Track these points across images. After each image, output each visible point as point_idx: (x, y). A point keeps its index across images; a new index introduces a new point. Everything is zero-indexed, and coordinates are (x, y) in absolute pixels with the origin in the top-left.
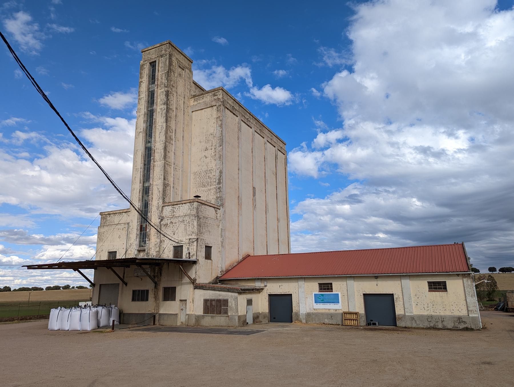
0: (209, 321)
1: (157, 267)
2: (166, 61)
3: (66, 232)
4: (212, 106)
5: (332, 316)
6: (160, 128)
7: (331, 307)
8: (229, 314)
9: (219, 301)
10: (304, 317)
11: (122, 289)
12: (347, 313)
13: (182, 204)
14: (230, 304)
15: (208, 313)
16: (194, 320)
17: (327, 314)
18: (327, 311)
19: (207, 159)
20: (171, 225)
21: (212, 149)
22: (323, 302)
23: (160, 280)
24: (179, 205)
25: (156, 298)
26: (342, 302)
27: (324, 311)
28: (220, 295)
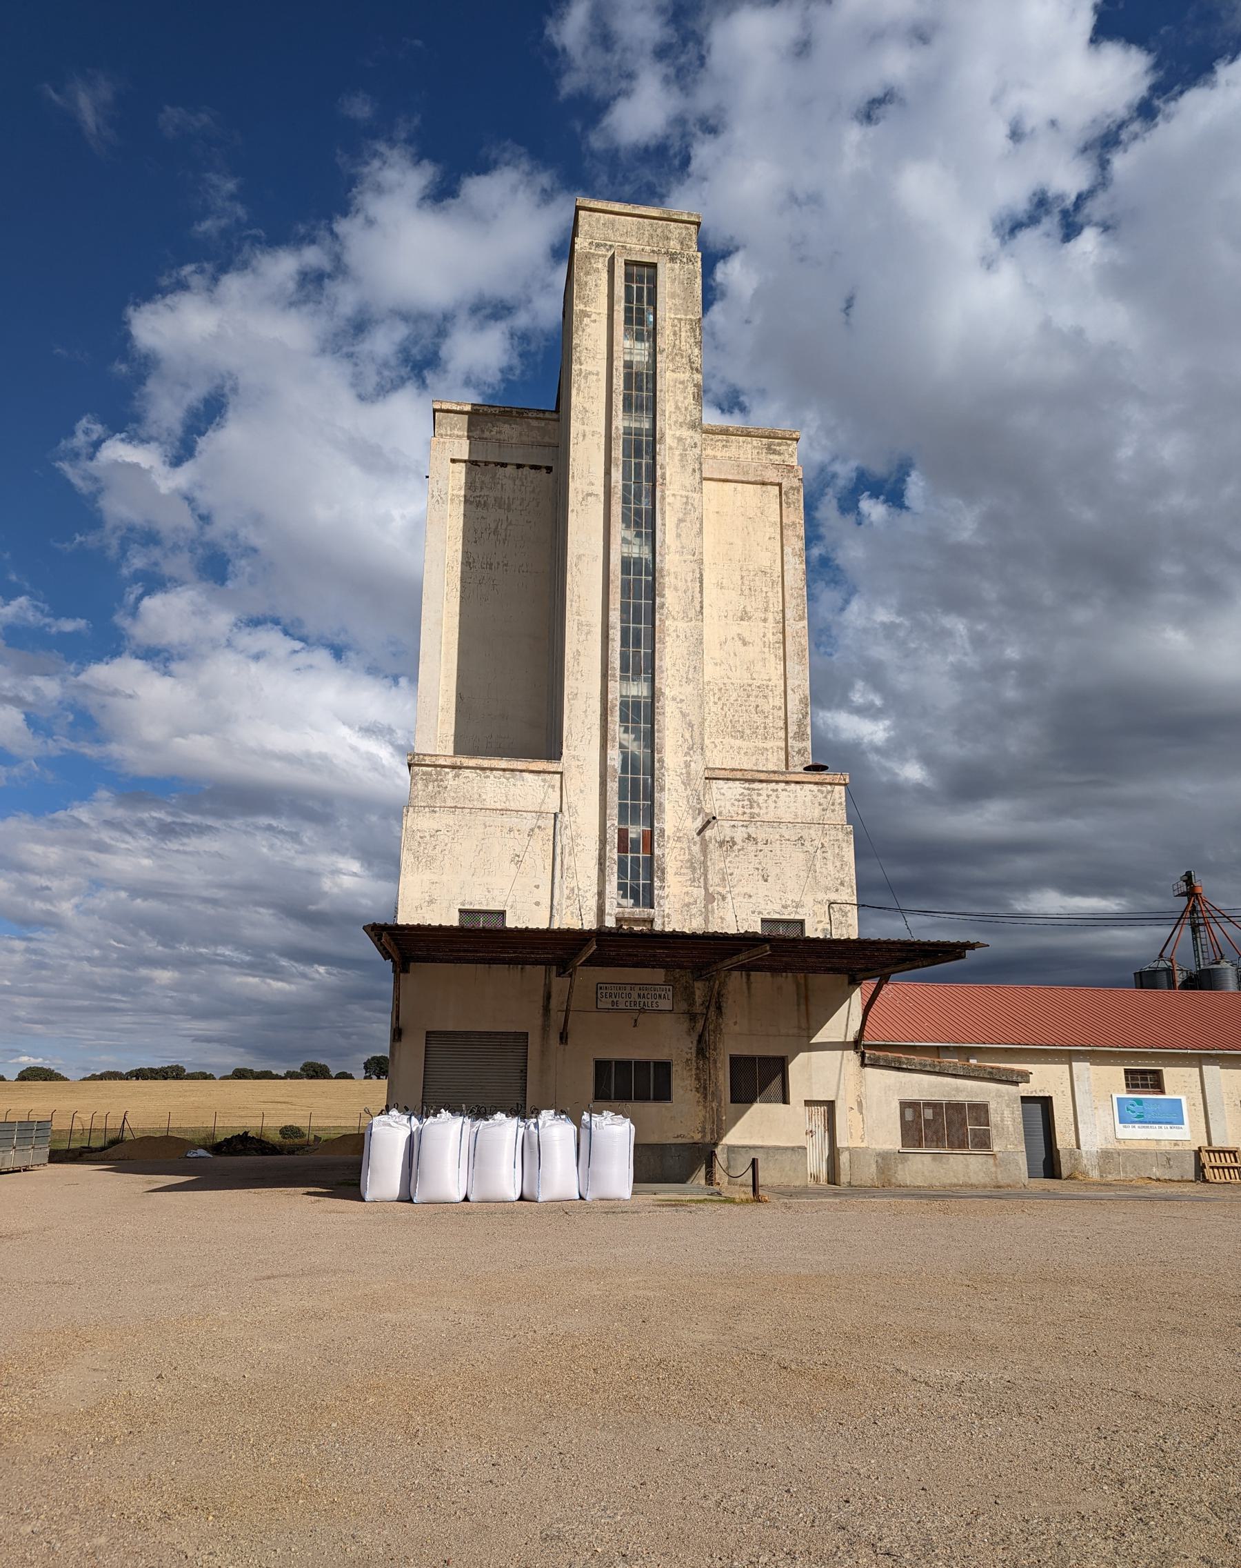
0: (923, 1167)
1: (698, 985)
2: (690, 281)
3: (203, 813)
4: (764, 484)
5: (1169, 1160)
6: (678, 503)
7: (1163, 1135)
8: (996, 1149)
9: (956, 1107)
10: (1095, 1161)
11: (543, 1053)
12: (1224, 1152)
13: (787, 782)
14: (994, 1118)
15: (920, 1146)
16: (874, 1168)
17: (1156, 1154)
18: (1153, 1146)
19: (750, 648)
20: (751, 847)
21: (765, 620)
22: (1142, 1120)
23: (718, 1029)
24: (773, 785)
25: (704, 1089)
26: (1190, 1122)
27: (1144, 1146)
28: (957, 1089)
